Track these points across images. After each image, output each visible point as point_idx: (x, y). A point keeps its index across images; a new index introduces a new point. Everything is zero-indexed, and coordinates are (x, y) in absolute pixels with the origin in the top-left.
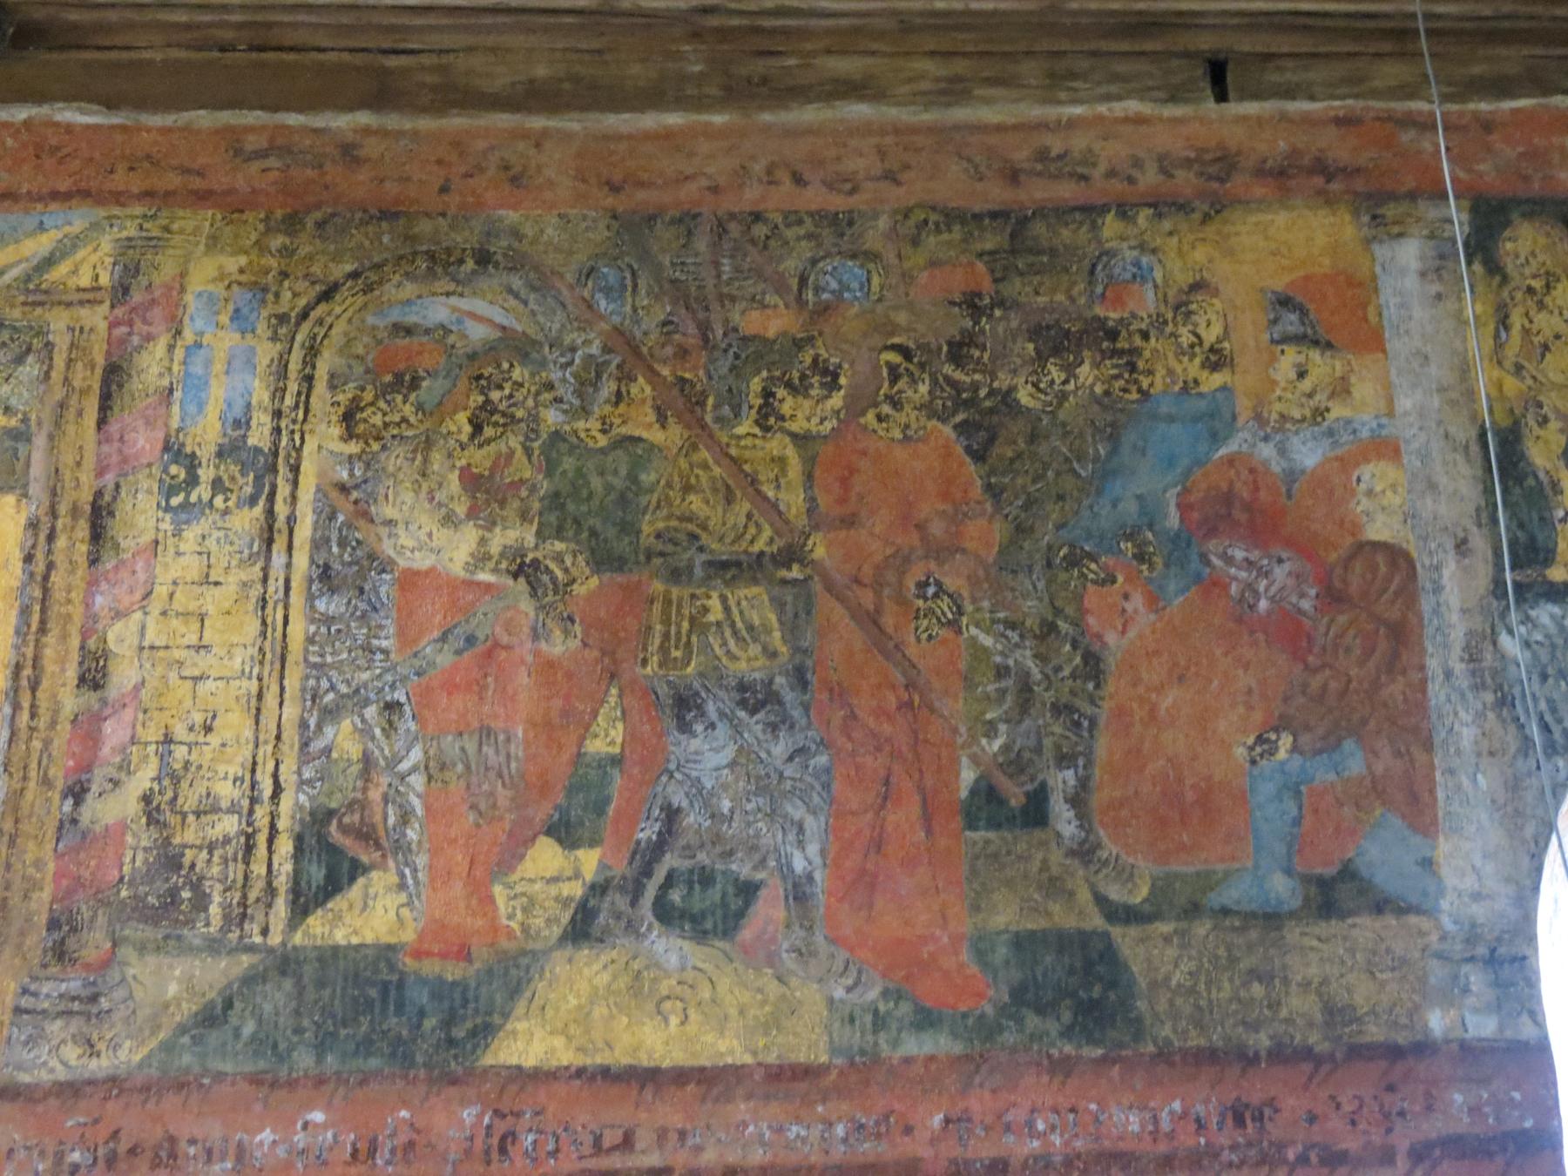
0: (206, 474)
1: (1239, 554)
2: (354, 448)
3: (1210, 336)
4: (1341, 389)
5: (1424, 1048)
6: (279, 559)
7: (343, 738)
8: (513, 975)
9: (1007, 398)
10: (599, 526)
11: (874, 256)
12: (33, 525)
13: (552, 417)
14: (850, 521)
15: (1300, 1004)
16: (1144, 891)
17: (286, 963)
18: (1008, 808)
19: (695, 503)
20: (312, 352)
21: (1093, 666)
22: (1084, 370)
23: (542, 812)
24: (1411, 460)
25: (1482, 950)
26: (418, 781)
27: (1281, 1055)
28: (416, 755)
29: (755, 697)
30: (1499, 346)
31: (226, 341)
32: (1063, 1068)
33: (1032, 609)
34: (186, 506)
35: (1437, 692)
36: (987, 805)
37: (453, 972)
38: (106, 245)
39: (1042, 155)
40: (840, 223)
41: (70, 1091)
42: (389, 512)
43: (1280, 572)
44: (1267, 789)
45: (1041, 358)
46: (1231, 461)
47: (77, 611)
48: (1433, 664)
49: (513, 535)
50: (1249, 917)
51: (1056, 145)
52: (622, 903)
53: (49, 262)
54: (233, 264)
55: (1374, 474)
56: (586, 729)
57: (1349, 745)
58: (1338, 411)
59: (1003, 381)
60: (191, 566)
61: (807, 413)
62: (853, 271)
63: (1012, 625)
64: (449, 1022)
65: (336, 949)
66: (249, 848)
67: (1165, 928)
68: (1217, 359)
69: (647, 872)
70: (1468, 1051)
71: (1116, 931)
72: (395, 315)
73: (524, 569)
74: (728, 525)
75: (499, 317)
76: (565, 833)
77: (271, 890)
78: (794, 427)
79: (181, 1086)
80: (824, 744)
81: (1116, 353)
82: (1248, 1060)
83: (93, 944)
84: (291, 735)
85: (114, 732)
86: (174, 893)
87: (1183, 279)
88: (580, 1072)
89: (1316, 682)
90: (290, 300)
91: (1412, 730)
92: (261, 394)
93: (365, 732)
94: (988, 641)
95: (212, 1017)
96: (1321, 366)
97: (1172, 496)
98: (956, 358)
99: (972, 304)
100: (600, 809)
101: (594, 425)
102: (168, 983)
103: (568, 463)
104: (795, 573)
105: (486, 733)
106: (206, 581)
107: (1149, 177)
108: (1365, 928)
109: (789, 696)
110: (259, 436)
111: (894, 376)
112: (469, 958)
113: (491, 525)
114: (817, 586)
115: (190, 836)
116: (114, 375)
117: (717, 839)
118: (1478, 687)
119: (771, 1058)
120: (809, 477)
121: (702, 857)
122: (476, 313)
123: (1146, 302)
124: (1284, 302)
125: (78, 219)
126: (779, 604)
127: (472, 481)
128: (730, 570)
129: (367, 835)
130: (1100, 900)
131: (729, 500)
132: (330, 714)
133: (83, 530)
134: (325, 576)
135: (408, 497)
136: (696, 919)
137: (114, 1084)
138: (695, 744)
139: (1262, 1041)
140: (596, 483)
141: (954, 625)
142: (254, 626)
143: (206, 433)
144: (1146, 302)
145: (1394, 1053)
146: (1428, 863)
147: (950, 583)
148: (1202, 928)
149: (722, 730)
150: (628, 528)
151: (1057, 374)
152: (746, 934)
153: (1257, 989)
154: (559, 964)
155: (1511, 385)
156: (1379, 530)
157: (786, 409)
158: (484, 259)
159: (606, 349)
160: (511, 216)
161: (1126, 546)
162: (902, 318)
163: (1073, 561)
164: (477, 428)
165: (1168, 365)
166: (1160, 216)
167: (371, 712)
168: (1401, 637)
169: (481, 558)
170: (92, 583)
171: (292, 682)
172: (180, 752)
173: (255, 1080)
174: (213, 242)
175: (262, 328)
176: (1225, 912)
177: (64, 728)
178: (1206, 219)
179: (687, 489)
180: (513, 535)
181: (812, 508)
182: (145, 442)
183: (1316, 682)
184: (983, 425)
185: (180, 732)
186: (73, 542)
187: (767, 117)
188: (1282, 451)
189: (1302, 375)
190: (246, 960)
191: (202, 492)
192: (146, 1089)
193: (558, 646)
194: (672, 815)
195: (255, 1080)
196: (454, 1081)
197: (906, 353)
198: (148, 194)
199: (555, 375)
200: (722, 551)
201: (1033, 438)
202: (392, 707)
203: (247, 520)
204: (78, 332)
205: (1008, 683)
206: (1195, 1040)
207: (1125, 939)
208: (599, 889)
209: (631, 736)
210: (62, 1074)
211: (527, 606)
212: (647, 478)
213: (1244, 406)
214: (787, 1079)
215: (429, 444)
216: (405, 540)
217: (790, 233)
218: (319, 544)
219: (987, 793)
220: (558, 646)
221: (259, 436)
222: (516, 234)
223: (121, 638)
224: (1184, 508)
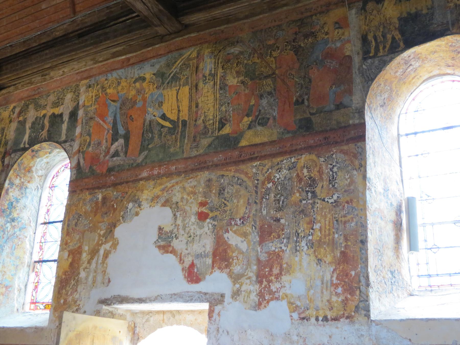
0: (207, 78)
1: (329, 61)
2: (223, 71)
3: (326, 31)
4: (343, 34)
5: (349, 126)
6: (216, 87)
7: (223, 108)
8: (241, 135)
9: (300, 46)
10: (252, 75)
11: (284, 30)
12: (190, 89)
13: (245, 62)
14: (280, 67)
15: (334, 122)
16: (315, 110)
17: (217, 137)
18: (299, 102)
19: (262, 69)
20: (218, 59)
21: (310, 81)
22: (310, 40)
23: (245, 114)
24: (352, 42)
25: (357, 111)
26: (231, 112)
27: (331, 130)
28: (231, 109)
29: (270, 93)
30: (365, 22)
31: (209, 60)
32: (304, 136)
33: (303, 74)
34: (206, 83)
35: (354, 75)
36: (297, 103)
37: (235, 135)
38: (196, 51)
39: (306, 9)
40: (279, 26)
41: (196, 157)
42: (228, 78)
43: (334, 63)
44: (331, 93)
45: (304, 39)
46: (328, 48)
47: (195, 98)
48: (354, 72)
49: (242, 78)
50: (328, 112)
51: (308, 7)
52: (254, 123)
53: (190, 55)
54: (209, 50)
55: (348, 46)
56: (250, 102)
57: (342, 85)
58: (343, 37)
59: (299, 43)
60: (206, 90)
61: (275, 54)
62: (281, 32)
63: (300, 77)
64: (235, 142)
65: (223, 135)
66: (214, 124)
67: (317, 115)
68: (327, 33)
69: (257, 119)
70: (354, 125)
71: (311, 116)
72: (227, 52)
73: (243, 82)
74: (266, 71)
75: (239, 49)
76: (248, 115)
77: (216, 129)
78: (274, 56)
79: (206, 154)
80: (277, 98)
81: (314, 36)
82: (327, 131)
83: (198, 139)
84: (218, 109)
85: (199, 112)
86: (206, 131)
87: (323, 22)
88: (249, 146)
89: (338, 77)
90: (216, 53)
91: (350, 82)
92: (213, 66)
93: (226, 107)
94: (297, 80)
95: (210, 145)
96: (341, 31)
97: (320, 55)
98: (294, 42)
99: (296, 34)
100: (252, 112)
101: (250, 61)
102: (205, 142)
103: (248, 67)
104: (274, 76)
105: (239, 104)
106: (208, 92)
107: (319, 9)
108: (342, 111)
109: (273, 93)
110: (213, 72)
111: (286, 46)
112: (237, 133)
113: (239, 77)
114: (277, 77)
115: (207, 124)
116: (197, 68)
117: (265, 113)
118: (359, 73)
119: (271, 140)
120: (276, 63)
121: (263, 116)
122: (235, 50)
123: (318, 27)
124: (336, 23)
125: (193, 49)
126: (272, 81)
127: (237, 72)
128: (266, 77)
129: (226, 120)
130: (310, 113)
131: (266, 68)
132: (222, 106)
133: (195, 88)
134: (221, 88)
135: (229, 76)
136: (262, 124)
137: (200, 155)
138: (263, 101)
139: (328, 128)
140: (251, 69)
141: (293, 79)
142: (213, 96)
143: (207, 72)
144: (318, 27)
145: (345, 127)
146: (351, 100)
147: (293, 73)
148: (322, 114)
149: (266, 98)
150: (255, 74)
151: (306, 41)
152: (268, 125)
153: (328, 121)
154: (247, 133)
155: (367, 28)
156: (347, 54)
157: (273, 54)
158: (237, 42)
159: (252, 51)
160: (241, 35)
161: (315, 63)
162: (287, 38)
163: (308, 67)
164: (237, 65)
165: (321, 36)
166: (320, 14)
167: (226, 104)
168: (349, 68)
169: (238, 82)
170: (196, 95)
171: (218, 102)
172: (206, 114)
173: (214, 152)
174: (208, 48)
175: (213, 58)
176: (325, 111)
177: (194, 113)
178: (326, 13)
179: (261, 67)
180: (242, 78)
181: (276, 67)
182: (201, 76)
183: (338, 77)
184: (297, 50)
185: (206, 111)
186: (194, 90)
187: (274, 12)
188: (335, 45)
189: (338, 33)
190: (213, 138)
191: (207, 80)
192: (203, 155)
193: (247, 91)
194: (260, 111)
195: (214, 152)
196: (235, 149)
197: (287, 42)
198: (200, 43)
199: (246, 56)
200: (265, 74)
201: (303, 50)
202: (229, 103)
203: (212, 83)
204: (193, 63)
205: (300, 85)
206: (320, 129)
207: (313, 119)
208: (251, 122)
209: (255, 101)
210: (195, 155)
211: (243, 87)
212: (257, 67)
213: (330, 40)
214: (272, 143)
215: (232, 69)
216: (229, 82)
217: (274, 29)
218: (220, 84)
219: (297, 101)
220: (247, 91)
221: (213, 72)
222: (241, 38)
223: (199, 101)
224: (322, 56)
